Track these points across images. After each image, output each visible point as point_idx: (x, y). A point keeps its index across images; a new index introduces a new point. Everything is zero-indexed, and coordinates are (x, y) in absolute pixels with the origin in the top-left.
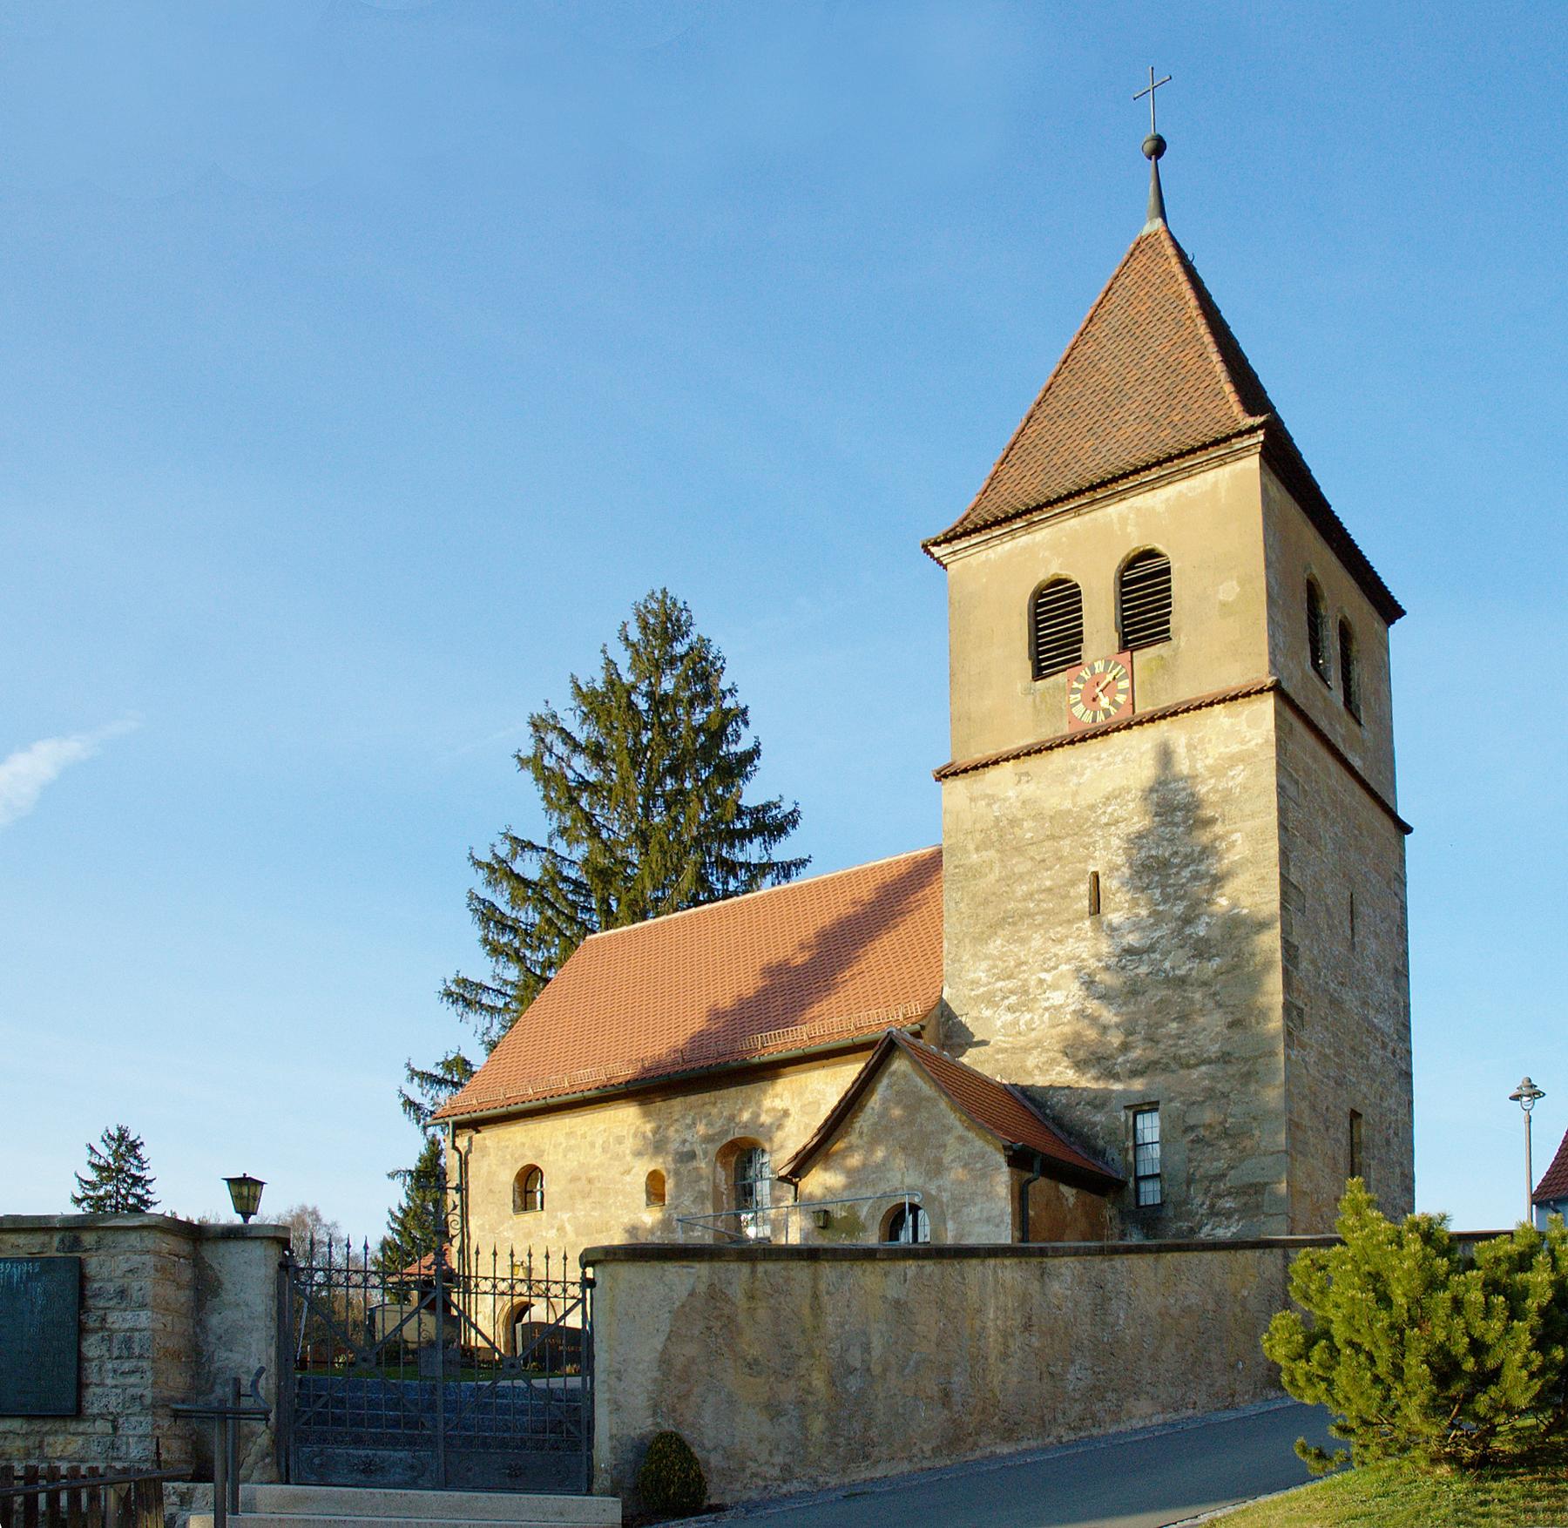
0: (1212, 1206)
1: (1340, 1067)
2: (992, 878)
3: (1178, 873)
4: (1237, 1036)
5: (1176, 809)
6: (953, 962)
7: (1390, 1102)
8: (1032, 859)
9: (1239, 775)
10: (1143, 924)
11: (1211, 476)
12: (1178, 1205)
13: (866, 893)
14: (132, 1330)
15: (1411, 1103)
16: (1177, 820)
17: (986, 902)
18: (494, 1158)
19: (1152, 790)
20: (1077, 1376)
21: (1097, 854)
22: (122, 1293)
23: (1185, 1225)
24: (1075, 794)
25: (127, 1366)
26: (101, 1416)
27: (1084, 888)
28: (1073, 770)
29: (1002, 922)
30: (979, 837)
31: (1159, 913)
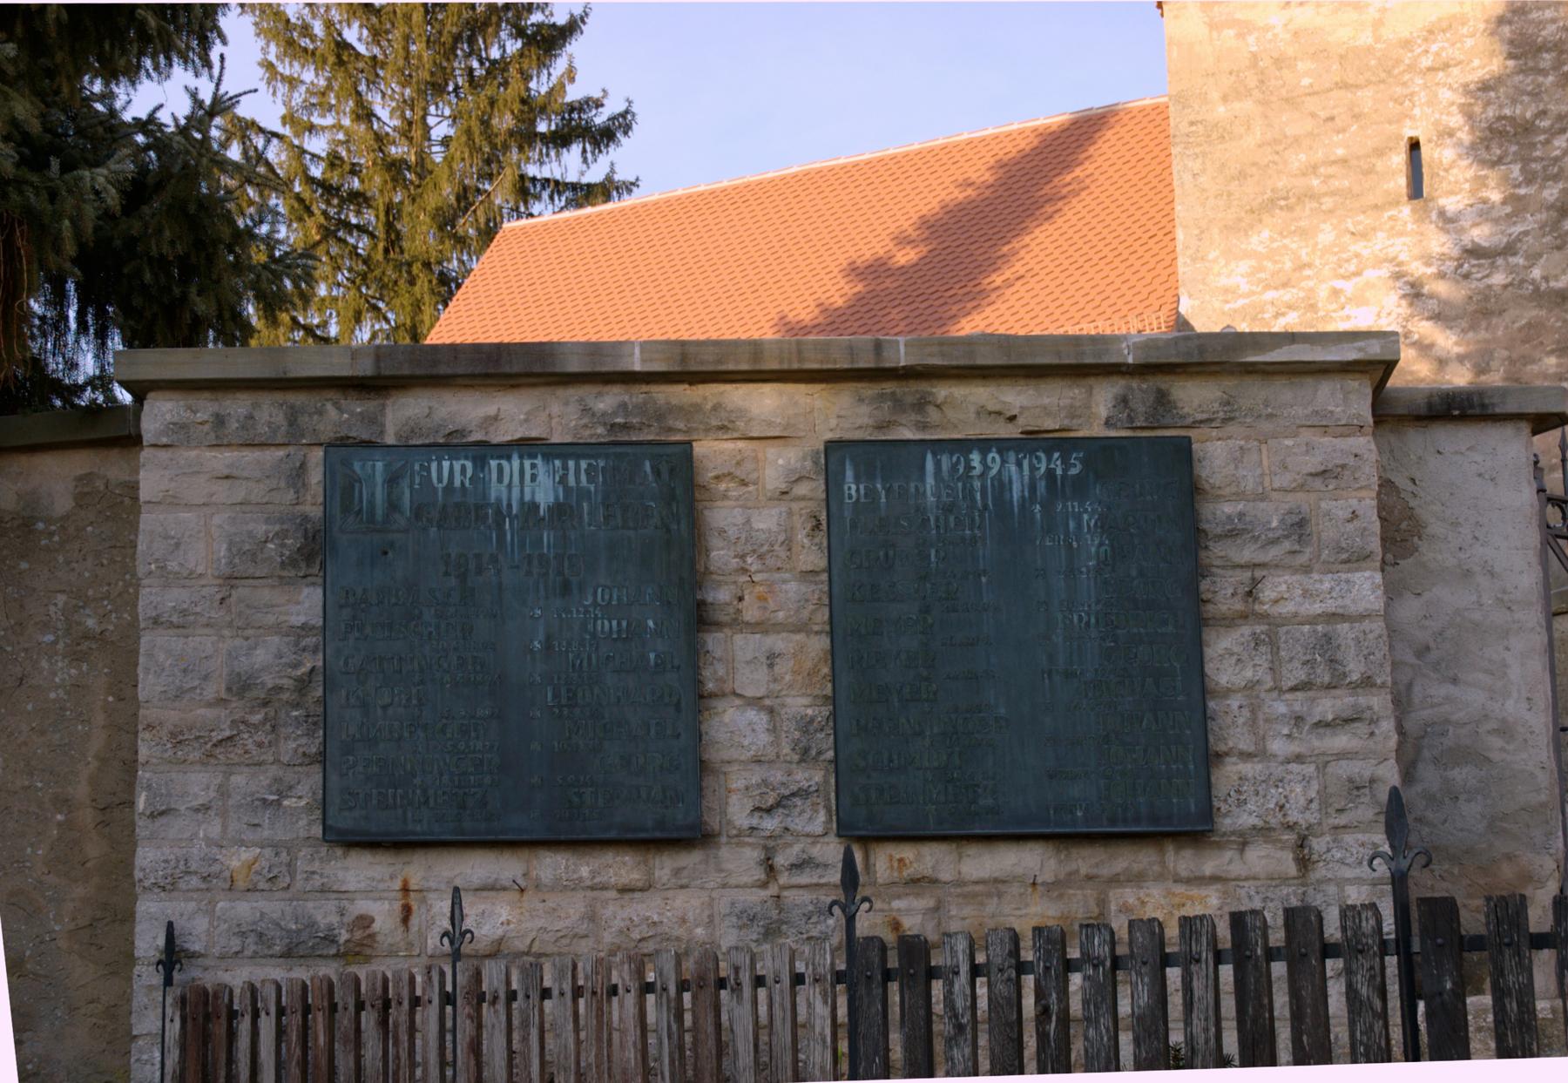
3: (1548, 142)
5: (1541, 48)
6: (1194, 260)
8: (1313, 115)
10: (1495, 214)
13: (980, 172)
14: (1333, 617)
16: (1542, 65)
17: (1242, 175)
19: (1501, 20)
21: (1417, 111)
22: (1299, 527)
24: (1378, 24)
25: (1327, 706)
26: (1264, 832)
29: (1271, 205)
31: (1519, 198)
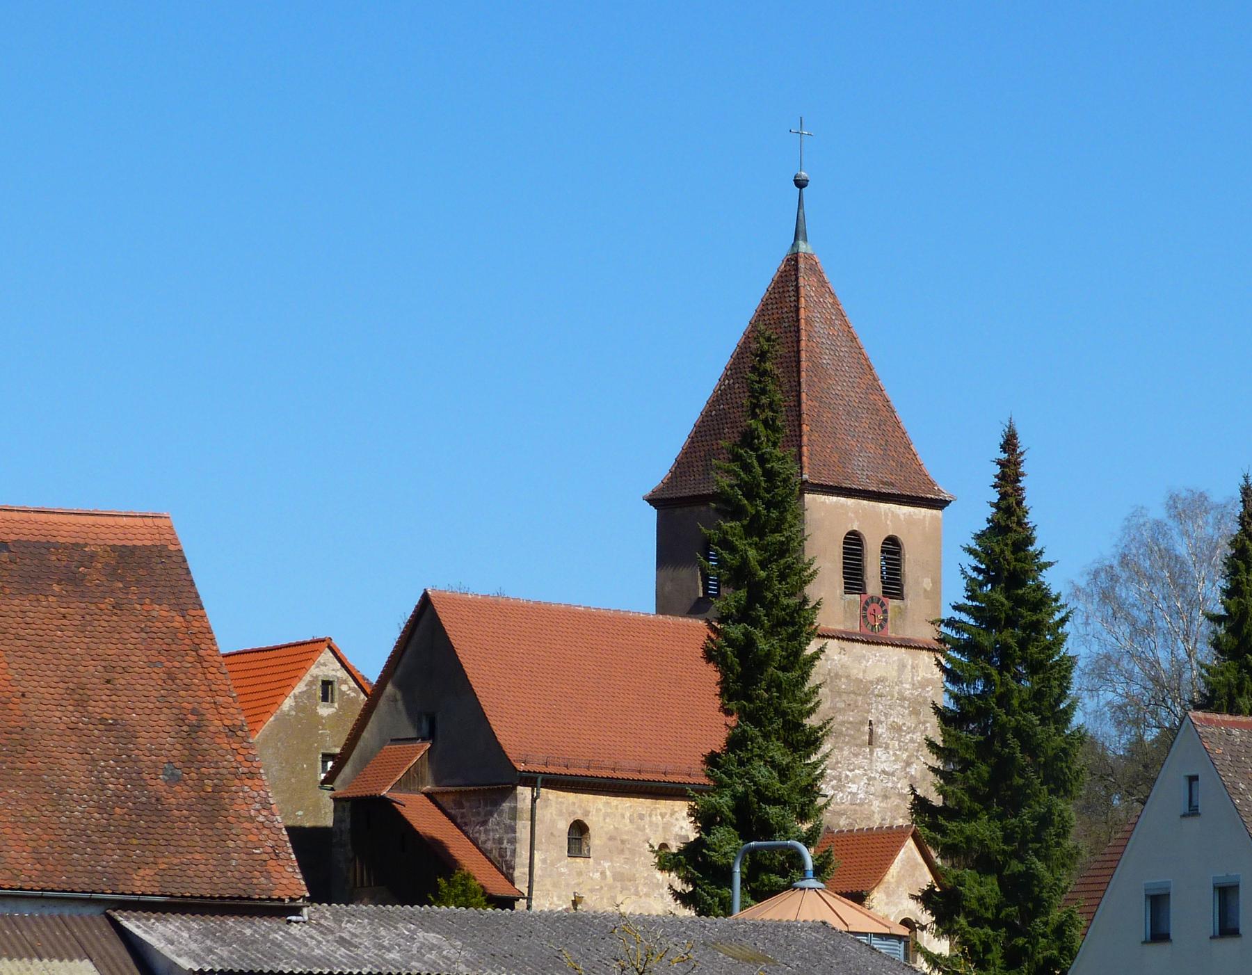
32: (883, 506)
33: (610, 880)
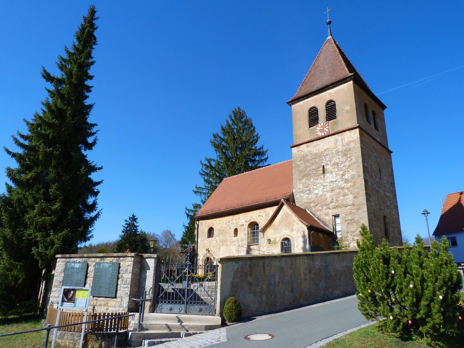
0: (353, 239)
1: (380, 206)
2: (303, 167)
4: (356, 200)
5: (339, 152)
7: (393, 213)
9: (352, 145)
11: (343, 86)
12: (345, 238)
15: (398, 213)
17: (301, 172)
18: (203, 226)
20: (322, 284)
23: (347, 243)
24: (318, 150)
27: (321, 169)
28: (318, 145)
29: (305, 176)
30: (299, 159)
32: (324, 94)
33: (219, 242)
